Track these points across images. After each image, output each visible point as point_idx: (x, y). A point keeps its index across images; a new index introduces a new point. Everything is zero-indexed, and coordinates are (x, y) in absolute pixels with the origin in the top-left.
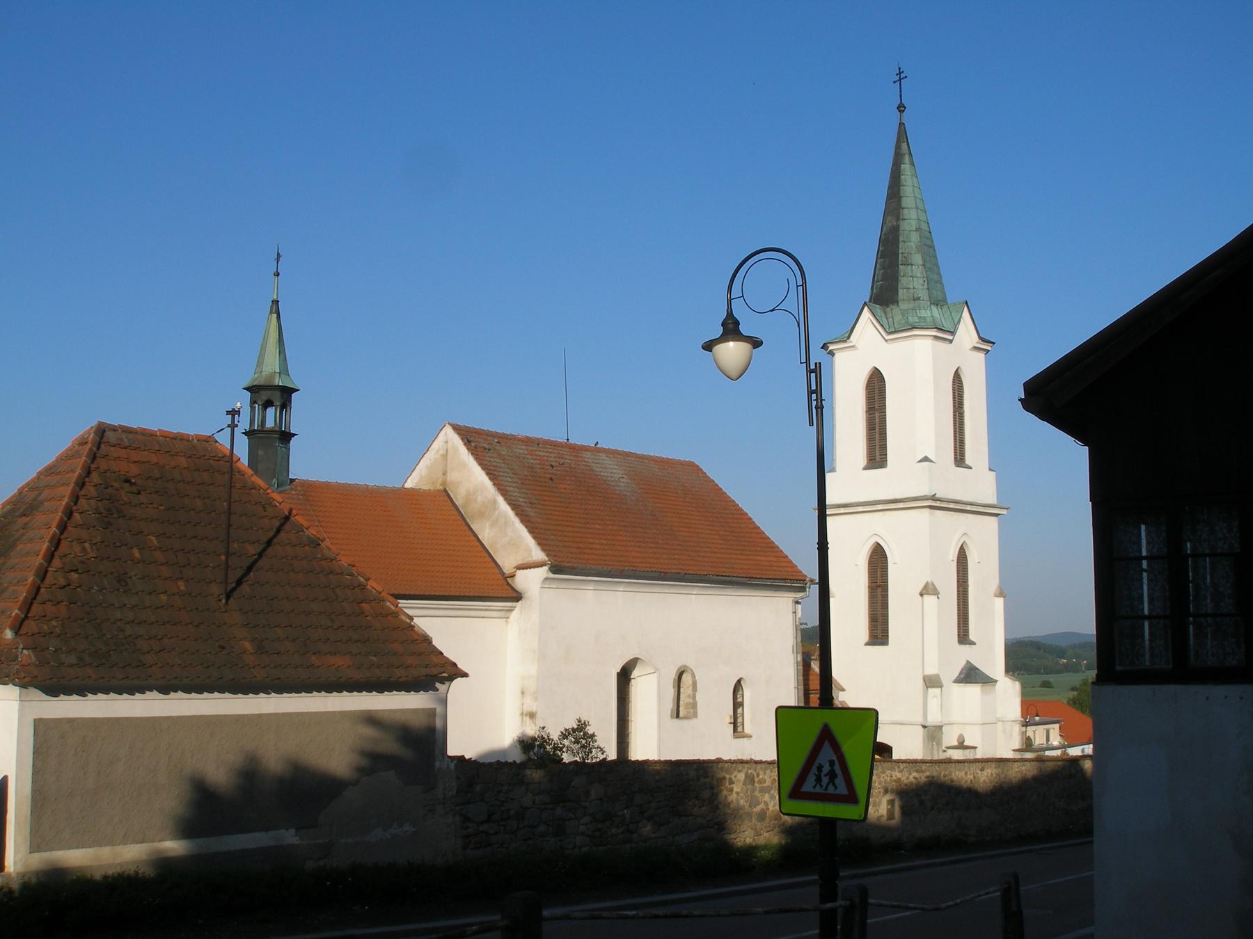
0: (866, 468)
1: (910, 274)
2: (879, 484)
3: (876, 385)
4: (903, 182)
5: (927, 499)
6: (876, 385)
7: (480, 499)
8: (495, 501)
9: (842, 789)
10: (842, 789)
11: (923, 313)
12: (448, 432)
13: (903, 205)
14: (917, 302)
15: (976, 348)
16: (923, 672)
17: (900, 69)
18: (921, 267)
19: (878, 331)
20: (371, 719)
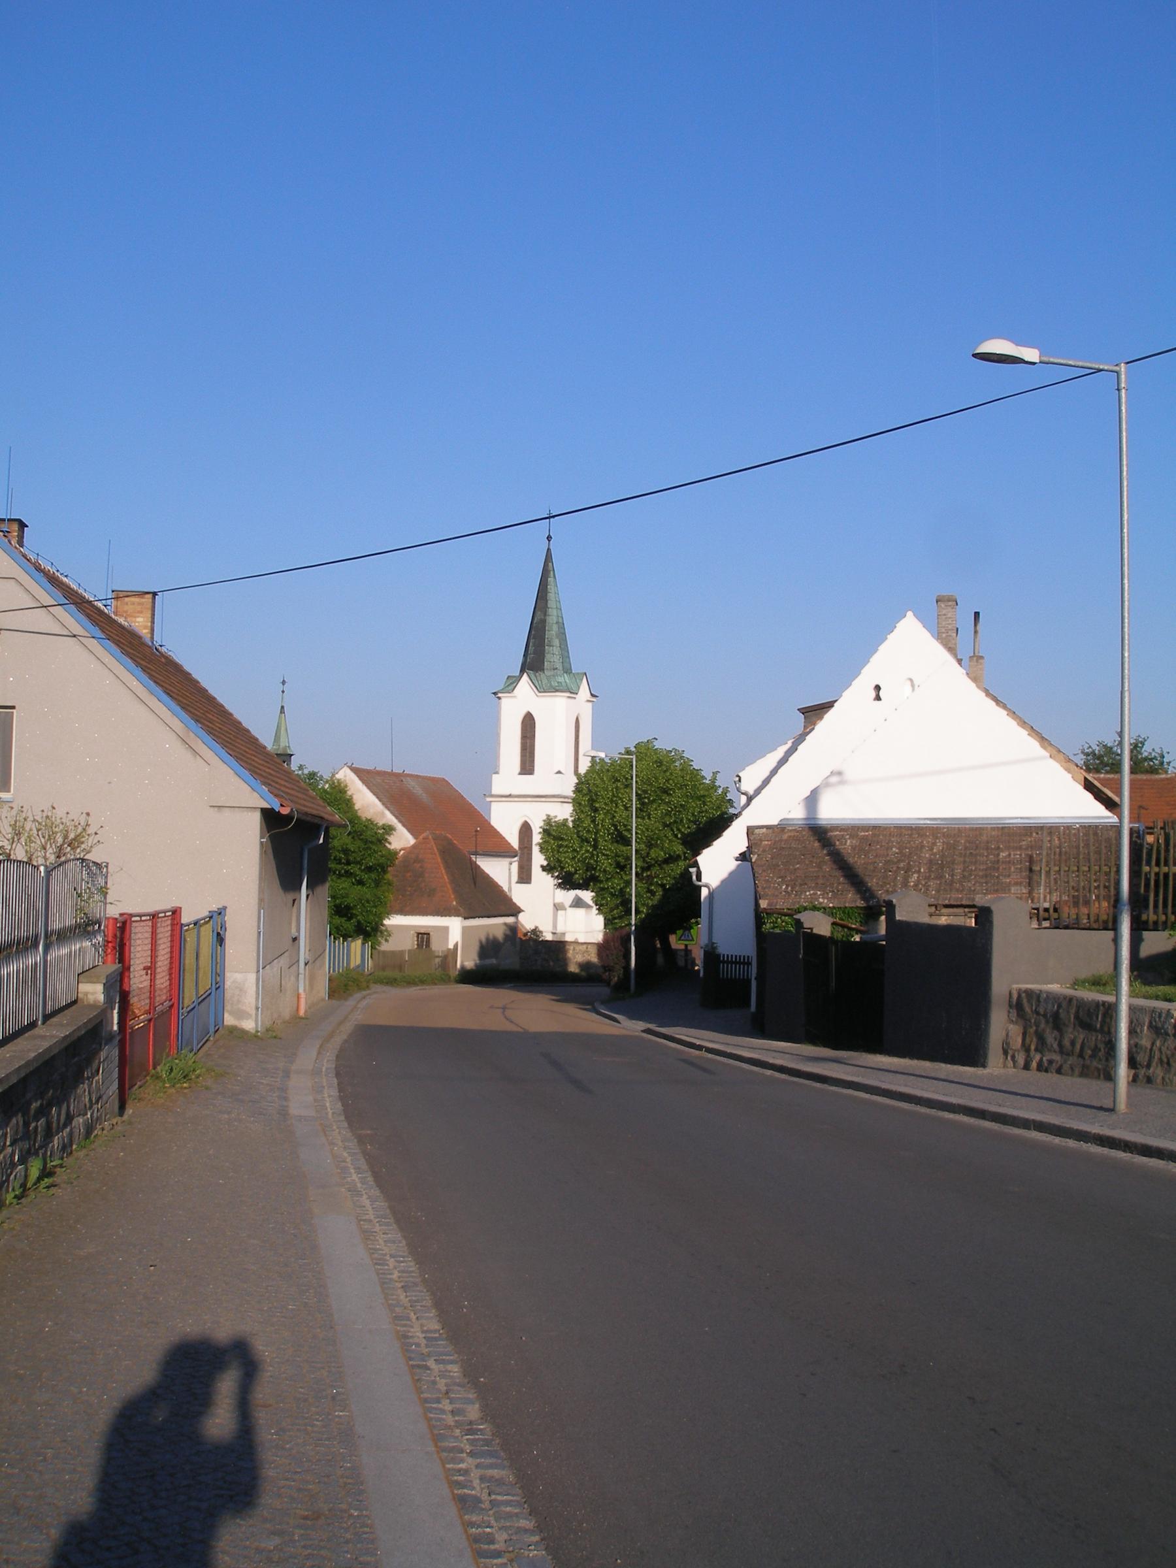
0: (520, 774)
1: (552, 652)
2: (527, 785)
3: (529, 723)
4: (549, 590)
5: (561, 797)
6: (529, 723)
7: (371, 811)
8: (383, 814)
9: (691, 938)
10: (691, 938)
11: (560, 679)
12: (347, 772)
13: (549, 606)
14: (555, 671)
15: (588, 701)
16: (554, 900)
17: (550, 511)
18: (559, 648)
19: (532, 688)
20: (505, 924)
